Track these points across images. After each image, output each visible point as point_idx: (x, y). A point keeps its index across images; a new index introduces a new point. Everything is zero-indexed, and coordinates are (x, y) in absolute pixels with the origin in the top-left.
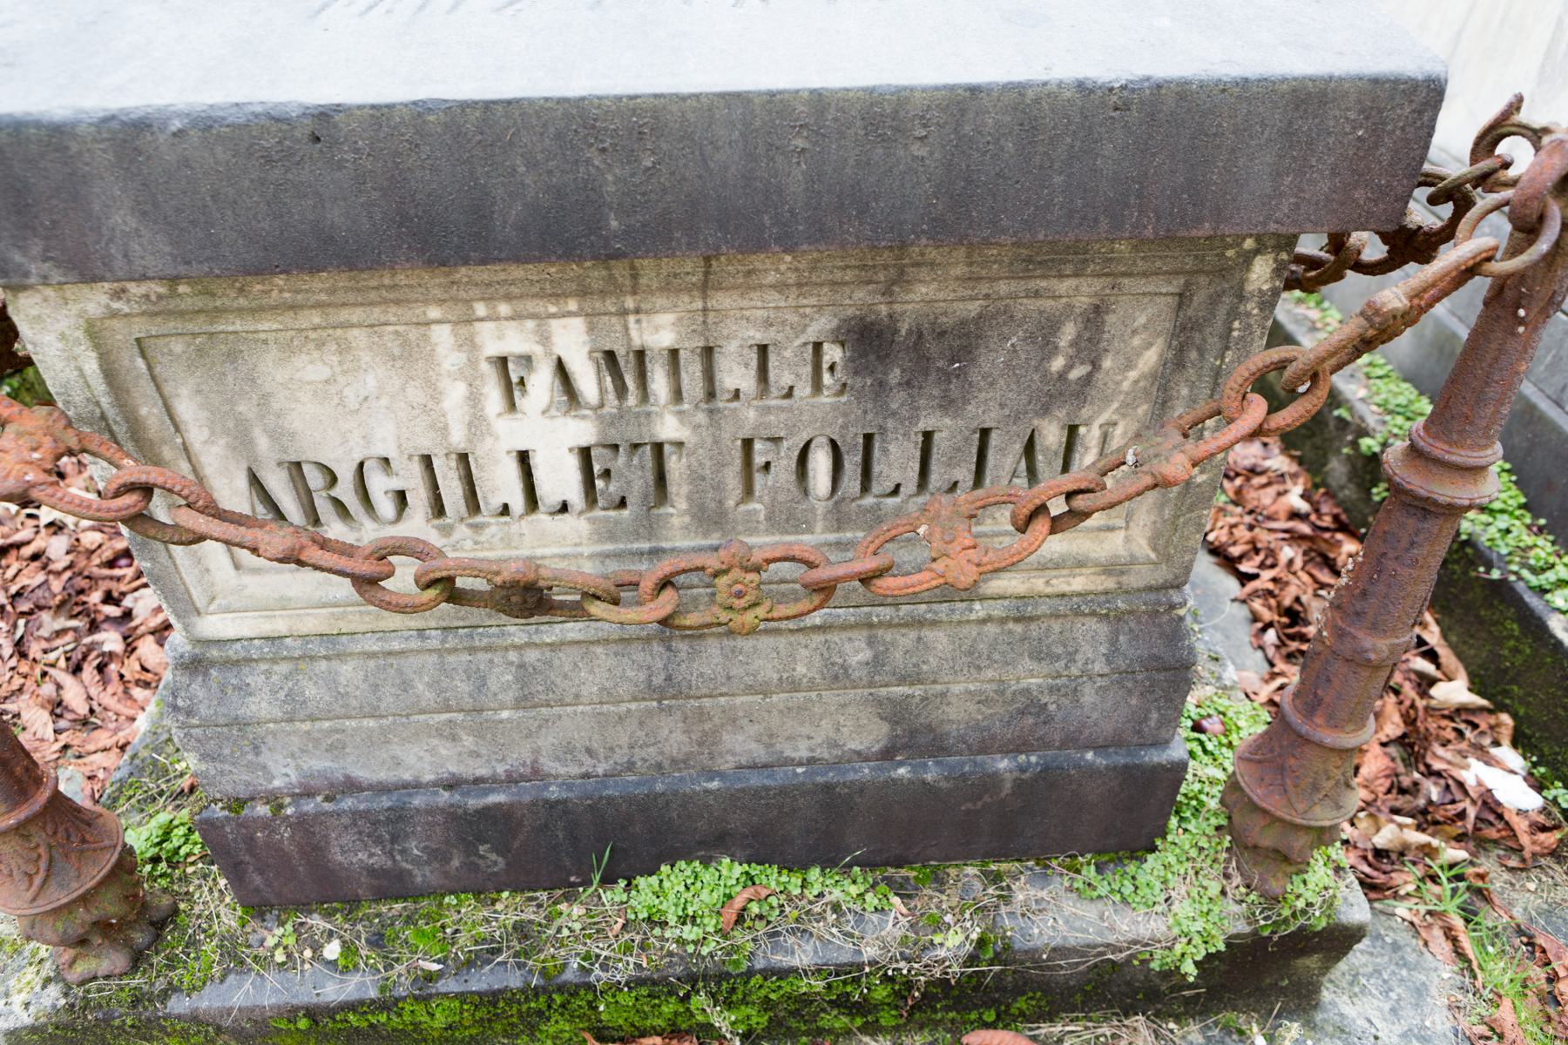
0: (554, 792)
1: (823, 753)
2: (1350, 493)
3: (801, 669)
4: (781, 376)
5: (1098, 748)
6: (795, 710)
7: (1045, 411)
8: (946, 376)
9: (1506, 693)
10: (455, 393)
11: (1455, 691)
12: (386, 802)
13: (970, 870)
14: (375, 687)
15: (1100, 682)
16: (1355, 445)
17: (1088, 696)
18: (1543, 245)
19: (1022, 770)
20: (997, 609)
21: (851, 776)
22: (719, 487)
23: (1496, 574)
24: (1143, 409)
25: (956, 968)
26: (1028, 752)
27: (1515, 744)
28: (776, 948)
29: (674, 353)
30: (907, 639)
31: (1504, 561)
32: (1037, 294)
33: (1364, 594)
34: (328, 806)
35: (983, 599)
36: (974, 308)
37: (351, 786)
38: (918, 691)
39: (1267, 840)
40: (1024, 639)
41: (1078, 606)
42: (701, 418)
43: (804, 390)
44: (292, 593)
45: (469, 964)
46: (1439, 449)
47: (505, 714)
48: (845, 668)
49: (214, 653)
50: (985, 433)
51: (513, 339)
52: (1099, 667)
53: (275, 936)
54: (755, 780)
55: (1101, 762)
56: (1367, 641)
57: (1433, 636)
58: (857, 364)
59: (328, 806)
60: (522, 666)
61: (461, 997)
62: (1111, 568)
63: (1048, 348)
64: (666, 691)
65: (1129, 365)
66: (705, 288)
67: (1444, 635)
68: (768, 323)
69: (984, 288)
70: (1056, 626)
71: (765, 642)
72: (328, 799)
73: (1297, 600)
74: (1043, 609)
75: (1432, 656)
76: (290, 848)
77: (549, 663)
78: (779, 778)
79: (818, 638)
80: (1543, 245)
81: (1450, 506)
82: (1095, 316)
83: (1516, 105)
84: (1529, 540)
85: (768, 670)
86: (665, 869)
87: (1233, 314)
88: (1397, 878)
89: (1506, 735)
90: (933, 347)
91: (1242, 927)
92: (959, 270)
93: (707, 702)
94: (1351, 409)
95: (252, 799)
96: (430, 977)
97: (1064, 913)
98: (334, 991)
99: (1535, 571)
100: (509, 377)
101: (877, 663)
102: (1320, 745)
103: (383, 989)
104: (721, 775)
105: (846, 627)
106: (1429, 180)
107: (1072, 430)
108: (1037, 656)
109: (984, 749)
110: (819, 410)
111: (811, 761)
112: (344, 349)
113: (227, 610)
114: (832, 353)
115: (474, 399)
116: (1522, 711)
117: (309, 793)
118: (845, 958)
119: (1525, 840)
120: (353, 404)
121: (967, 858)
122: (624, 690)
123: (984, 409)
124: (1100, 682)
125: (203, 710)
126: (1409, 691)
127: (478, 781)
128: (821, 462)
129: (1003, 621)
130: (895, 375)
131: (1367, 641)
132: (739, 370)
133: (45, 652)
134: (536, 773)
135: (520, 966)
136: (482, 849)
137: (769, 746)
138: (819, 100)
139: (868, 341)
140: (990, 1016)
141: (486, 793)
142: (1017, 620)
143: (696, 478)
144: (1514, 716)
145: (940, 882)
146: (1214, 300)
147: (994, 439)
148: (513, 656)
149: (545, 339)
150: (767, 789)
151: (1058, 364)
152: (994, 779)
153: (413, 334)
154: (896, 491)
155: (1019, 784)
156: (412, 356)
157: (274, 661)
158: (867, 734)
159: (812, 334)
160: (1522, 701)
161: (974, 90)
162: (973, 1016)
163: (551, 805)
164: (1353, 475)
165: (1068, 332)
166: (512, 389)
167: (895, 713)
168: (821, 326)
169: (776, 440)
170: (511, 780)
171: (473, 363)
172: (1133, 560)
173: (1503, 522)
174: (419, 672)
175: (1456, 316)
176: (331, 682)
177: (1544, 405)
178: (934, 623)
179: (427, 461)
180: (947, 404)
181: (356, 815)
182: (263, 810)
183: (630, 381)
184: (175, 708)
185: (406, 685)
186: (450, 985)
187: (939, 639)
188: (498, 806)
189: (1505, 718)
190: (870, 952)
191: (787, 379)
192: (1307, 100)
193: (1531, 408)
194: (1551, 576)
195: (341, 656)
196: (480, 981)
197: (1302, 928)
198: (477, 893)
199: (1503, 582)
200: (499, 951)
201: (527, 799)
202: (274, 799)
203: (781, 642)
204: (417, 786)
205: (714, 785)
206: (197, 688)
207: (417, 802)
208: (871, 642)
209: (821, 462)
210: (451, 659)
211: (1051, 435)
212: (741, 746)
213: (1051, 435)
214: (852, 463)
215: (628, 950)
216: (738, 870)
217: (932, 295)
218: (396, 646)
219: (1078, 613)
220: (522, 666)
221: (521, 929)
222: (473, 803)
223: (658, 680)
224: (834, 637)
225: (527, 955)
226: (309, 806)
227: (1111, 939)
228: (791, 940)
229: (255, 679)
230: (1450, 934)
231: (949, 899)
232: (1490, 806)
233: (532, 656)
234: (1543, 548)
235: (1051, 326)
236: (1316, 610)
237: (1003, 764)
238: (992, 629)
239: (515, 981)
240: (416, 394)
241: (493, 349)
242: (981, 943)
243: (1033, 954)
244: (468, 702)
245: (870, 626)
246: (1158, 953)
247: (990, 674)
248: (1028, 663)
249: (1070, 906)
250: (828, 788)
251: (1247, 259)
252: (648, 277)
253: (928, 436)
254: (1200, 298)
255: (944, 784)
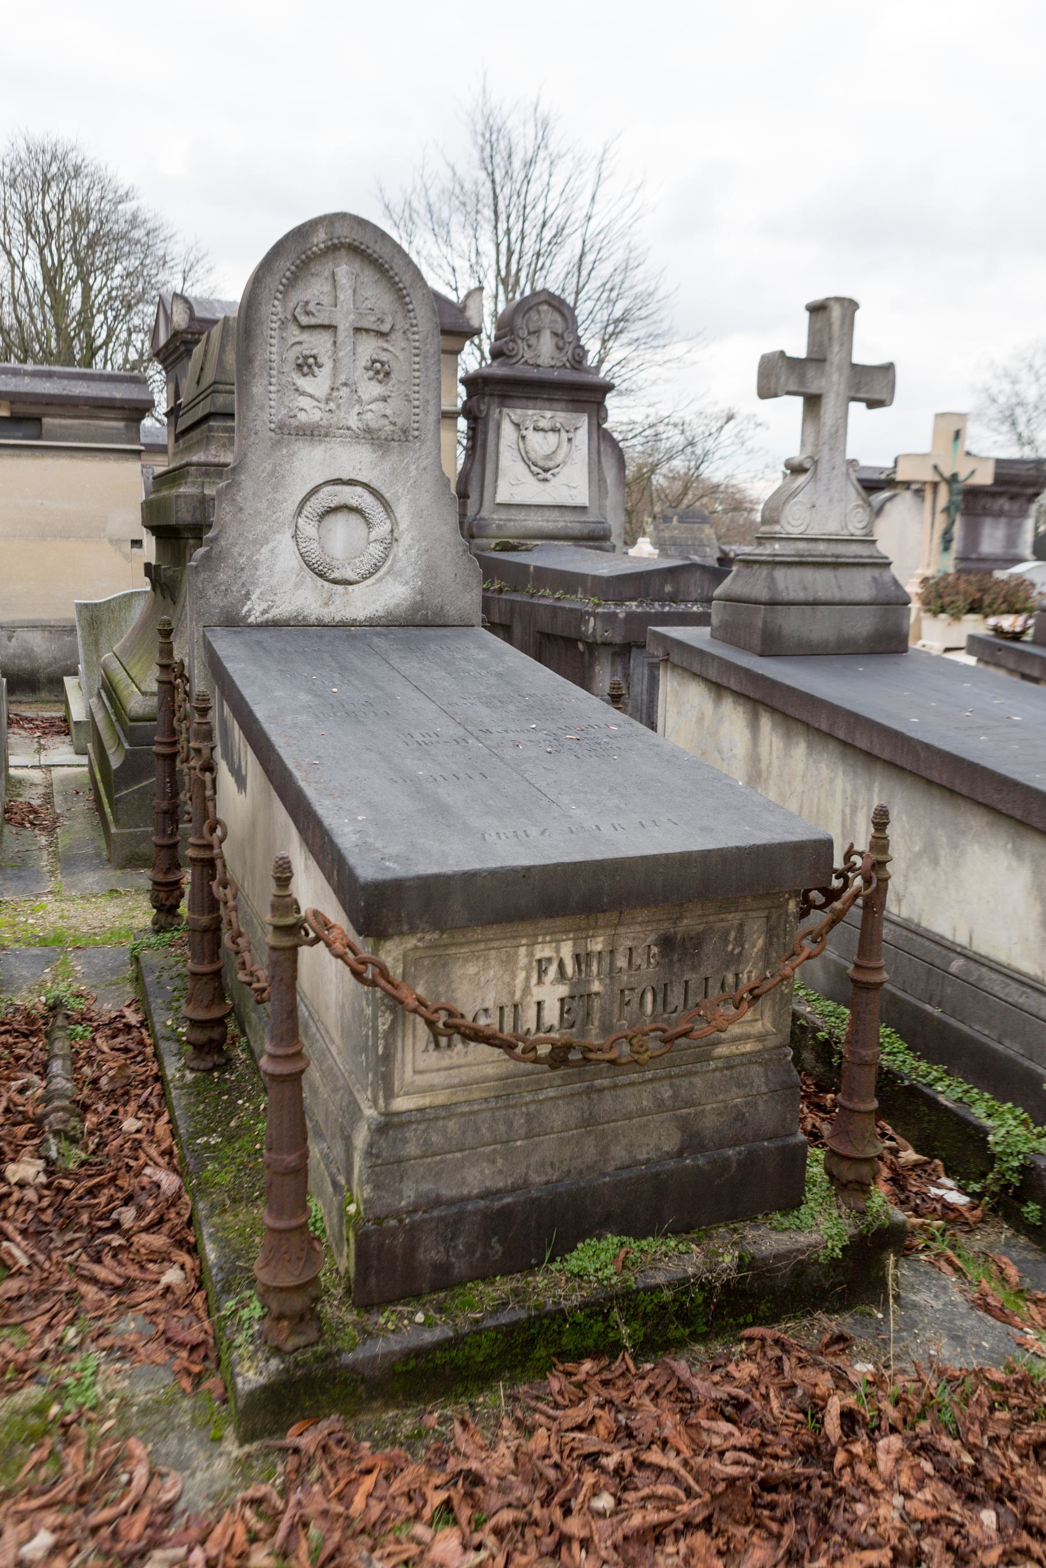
0: (534, 1194)
1: (653, 1155)
2: (819, 1069)
3: (645, 1103)
4: (637, 960)
5: (769, 1139)
6: (640, 1131)
7: (727, 968)
8: (693, 956)
9: (933, 1149)
10: (522, 975)
11: (910, 1155)
12: (454, 1209)
13: (721, 1230)
14: (464, 1133)
15: (765, 1098)
16: (814, 1038)
17: (761, 1107)
18: (874, 885)
19: (740, 1154)
20: (720, 1064)
21: (667, 1167)
22: (611, 1014)
23: (907, 1083)
24: (760, 964)
25: (733, 1274)
26: (739, 1145)
27: (947, 1176)
28: (646, 1277)
29: (600, 953)
30: (685, 1083)
31: (908, 1076)
32: (722, 920)
33: (857, 1031)
34: (426, 1216)
35: (713, 1059)
36: (702, 927)
37: (437, 1202)
38: (692, 1110)
39: (851, 1175)
40: (731, 1078)
41: (749, 1059)
42: (607, 981)
43: (644, 966)
44: (435, 1082)
45: (496, 1312)
46: (865, 963)
47: (519, 1143)
48: (662, 1100)
49: (396, 1119)
50: (706, 979)
51: (543, 951)
52: (764, 1089)
53: (384, 1319)
54: (625, 1174)
55: (772, 1145)
56: (864, 1053)
57: (890, 1131)
58: (663, 954)
59: (426, 1216)
60: (528, 1114)
61: (497, 1328)
62: (760, 1038)
63: (726, 942)
64: (589, 1122)
65: (754, 946)
66: (616, 926)
67: (894, 1129)
68: (634, 939)
69: (705, 919)
70: (743, 1070)
71: (629, 1091)
72: (424, 1212)
73: (814, 1126)
74: (737, 1061)
75: (891, 1139)
76: (399, 1251)
77: (539, 1111)
78: (635, 1172)
79: (650, 1087)
80: (874, 885)
81: (875, 984)
82: (741, 928)
83: (852, 846)
84: (916, 1064)
85: (631, 1105)
86: (580, 1245)
87: (786, 922)
88: (916, 1242)
89: (941, 1169)
90: (688, 944)
91: (853, 1231)
92: (699, 912)
93: (606, 1126)
94: (806, 1019)
95: (387, 1217)
96: (477, 1321)
97: (772, 1239)
98: (428, 1337)
99: (924, 1077)
100: (542, 967)
101: (675, 1096)
102: (859, 1112)
103: (456, 1331)
104: (609, 1175)
105: (661, 1079)
106: (835, 871)
107: (737, 975)
108: (739, 1086)
109: (721, 1147)
110: (649, 970)
111: (648, 1161)
112: (486, 959)
113: (407, 1094)
114: (655, 950)
115: (528, 979)
116: (944, 1154)
117: (415, 1211)
118: (681, 1275)
119: (967, 1215)
120: (482, 984)
121: (719, 1222)
122: (572, 1123)
123: (706, 970)
124: (765, 1098)
125: (384, 1154)
126: (889, 1157)
127: (498, 1191)
128: (649, 997)
129: (722, 1069)
130: (676, 957)
131: (864, 1053)
132: (623, 959)
133: (64, 1256)
134: (526, 1184)
135: (523, 1307)
136: (494, 1240)
137: (631, 1152)
138: (667, 856)
139: (667, 943)
140: (750, 1318)
141: (501, 1199)
142: (727, 1068)
143: (603, 1009)
144: (941, 1159)
145: (710, 1237)
146: (779, 917)
147: (711, 982)
148: (524, 1109)
149: (558, 950)
150: (630, 1179)
151: (730, 947)
152: (728, 1159)
153: (512, 951)
154: (674, 1011)
155: (740, 1163)
156: (509, 962)
157: (419, 1122)
158: (671, 1142)
159: (648, 943)
160: (944, 1149)
161: (709, 851)
162: (741, 1320)
163: (533, 1201)
164: (819, 1058)
165: (733, 935)
166: (542, 972)
167: (684, 1125)
168: (652, 937)
169: (632, 989)
170: (513, 1189)
171: (530, 963)
172: (768, 1034)
173: (901, 1057)
174: (483, 1122)
175: (856, 913)
176: (444, 1131)
177: (899, 993)
178: (696, 1073)
179: (501, 1009)
180: (694, 968)
181: (441, 1219)
182: (393, 1222)
183: (583, 967)
184: (371, 1154)
185: (477, 1130)
186: (490, 1323)
187: (697, 1081)
188: (509, 1204)
189: (937, 1161)
190: (691, 1270)
191: (639, 962)
192: (798, 847)
193: (894, 995)
194: (931, 1077)
195: (449, 1117)
196: (505, 1318)
197: (879, 1229)
198: (483, 1280)
199: (911, 1085)
200: (508, 1303)
201: (522, 1199)
202: (397, 1214)
203: (635, 1090)
204: (467, 1199)
205: (607, 1179)
206: (383, 1143)
207: (470, 1207)
208: (671, 1086)
209: (649, 997)
210: (497, 1113)
211: (730, 979)
212: (619, 1153)
213: (730, 979)
214: (660, 999)
215: (574, 1290)
216: (616, 1240)
217: (689, 924)
218: (476, 1107)
219: (751, 1063)
220: (528, 1114)
221: (515, 1292)
222: (497, 1205)
223: (586, 1115)
224: (657, 1085)
225: (524, 1301)
226: (418, 1216)
227: (798, 1246)
228: (651, 1273)
229: (409, 1134)
230: (950, 1263)
231: (717, 1242)
232: (948, 1207)
233: (532, 1108)
234: (923, 1066)
235: (727, 933)
236: (826, 1129)
237: (731, 1152)
238: (718, 1074)
239: (523, 1315)
240: (507, 978)
241: (538, 956)
242: (741, 1258)
243: (764, 1259)
244: (505, 1137)
245: (671, 1077)
246: (821, 1252)
247: (721, 1097)
248: (735, 1090)
249: (774, 1236)
250: (658, 1174)
251: (787, 900)
252: (601, 922)
253: (686, 982)
254: (774, 917)
255: (707, 1167)
